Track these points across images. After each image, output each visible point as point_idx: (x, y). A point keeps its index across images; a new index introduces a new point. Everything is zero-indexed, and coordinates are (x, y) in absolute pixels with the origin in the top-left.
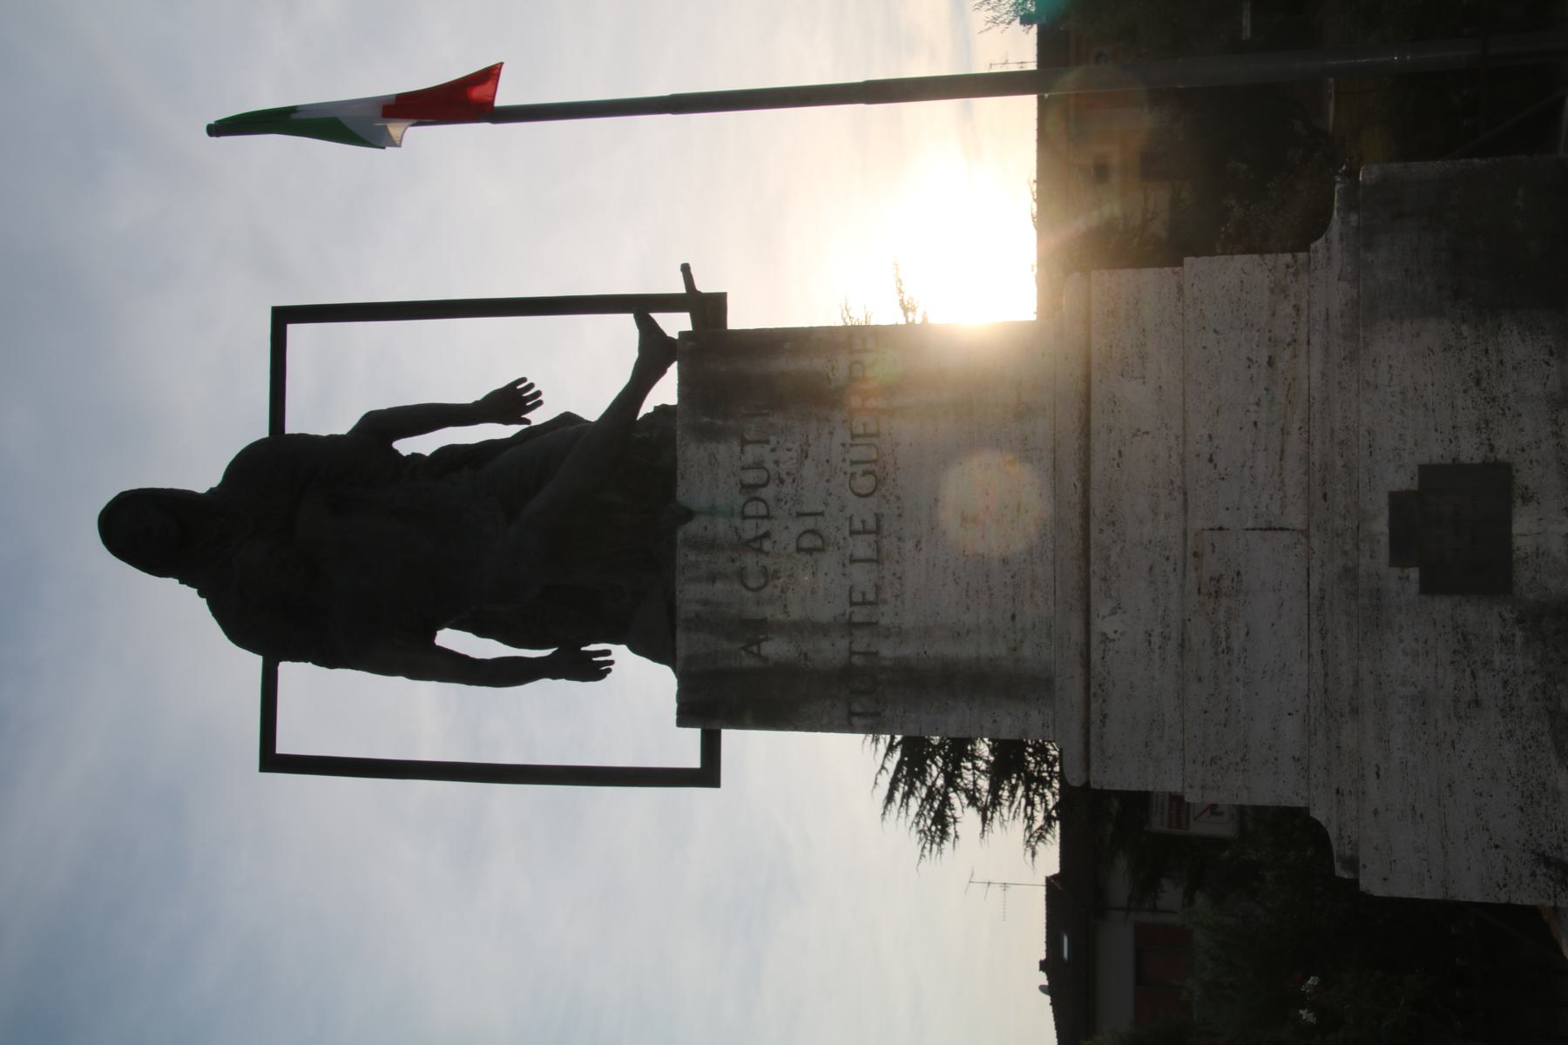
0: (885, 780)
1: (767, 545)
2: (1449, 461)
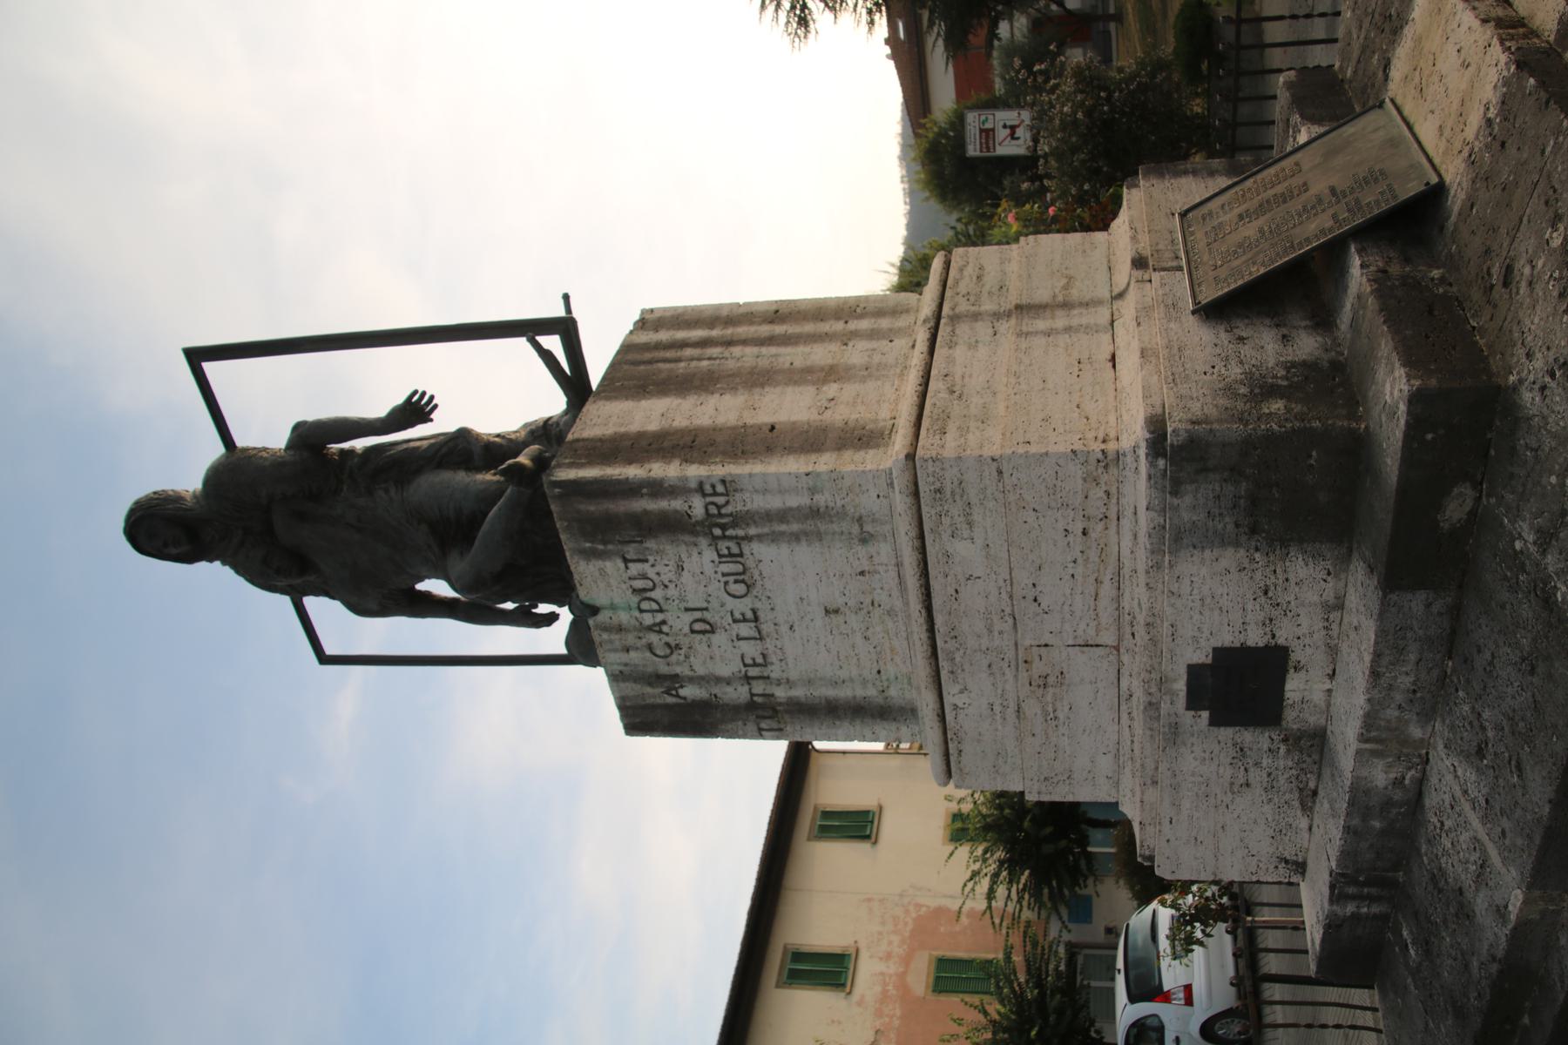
1: (665, 629)
2: (1238, 645)
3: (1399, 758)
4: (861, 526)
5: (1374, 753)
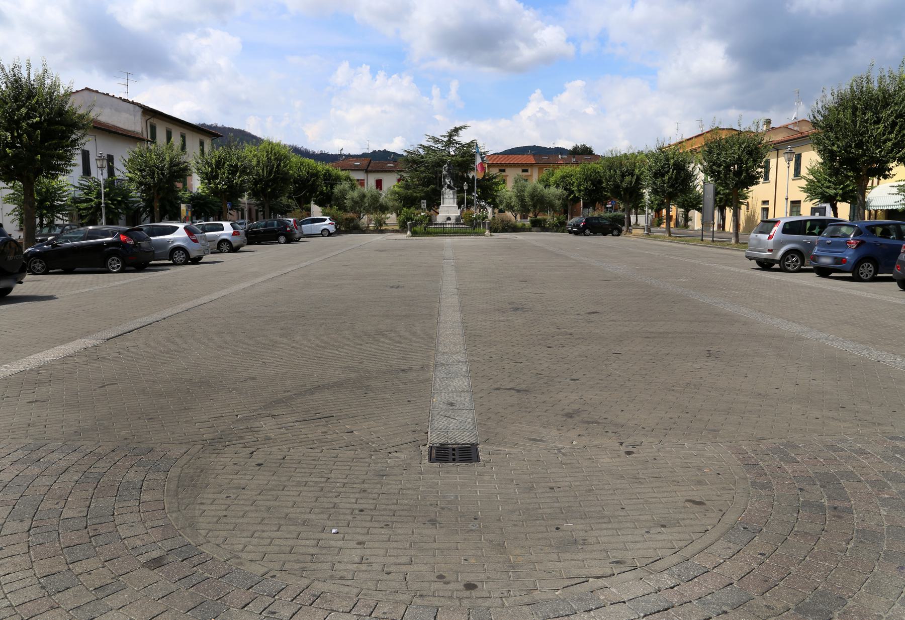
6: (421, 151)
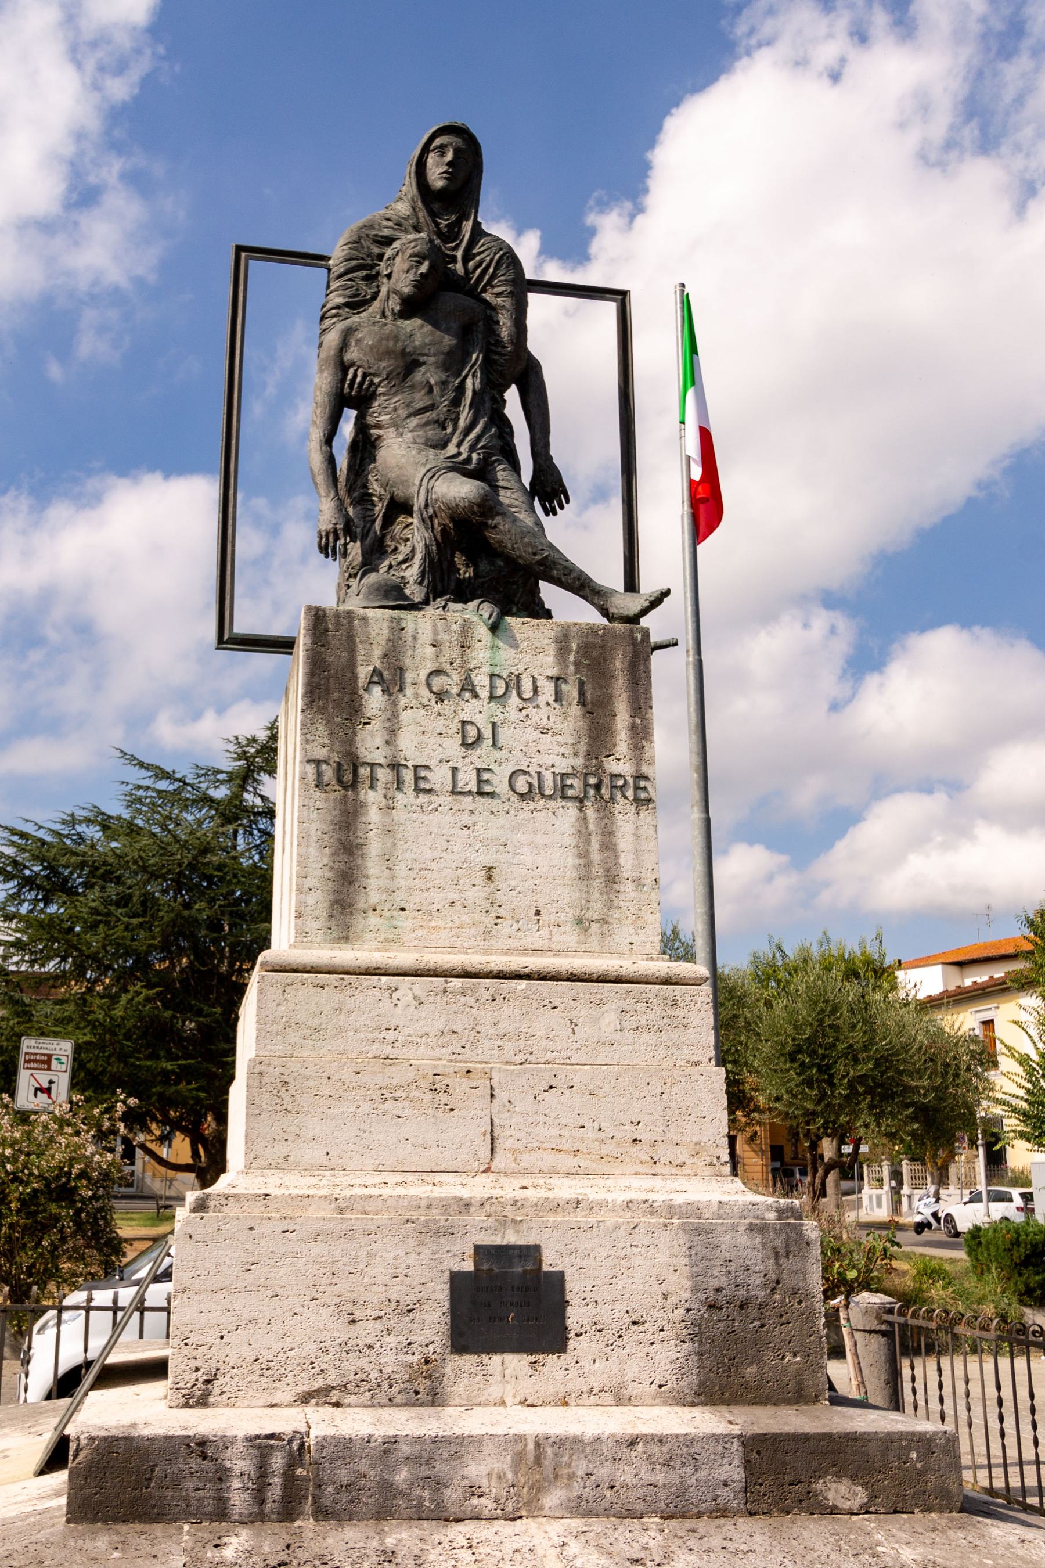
0: (30, 829)
2: (568, 1298)
3: (513, 1486)
4: (598, 921)
5: (519, 1459)
6: (93, 833)
